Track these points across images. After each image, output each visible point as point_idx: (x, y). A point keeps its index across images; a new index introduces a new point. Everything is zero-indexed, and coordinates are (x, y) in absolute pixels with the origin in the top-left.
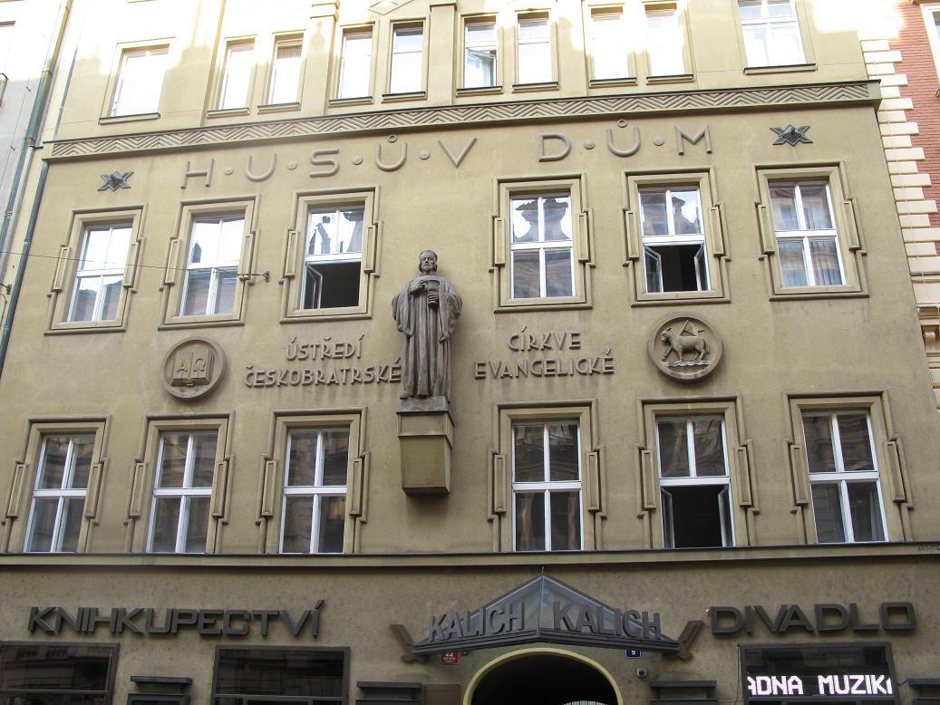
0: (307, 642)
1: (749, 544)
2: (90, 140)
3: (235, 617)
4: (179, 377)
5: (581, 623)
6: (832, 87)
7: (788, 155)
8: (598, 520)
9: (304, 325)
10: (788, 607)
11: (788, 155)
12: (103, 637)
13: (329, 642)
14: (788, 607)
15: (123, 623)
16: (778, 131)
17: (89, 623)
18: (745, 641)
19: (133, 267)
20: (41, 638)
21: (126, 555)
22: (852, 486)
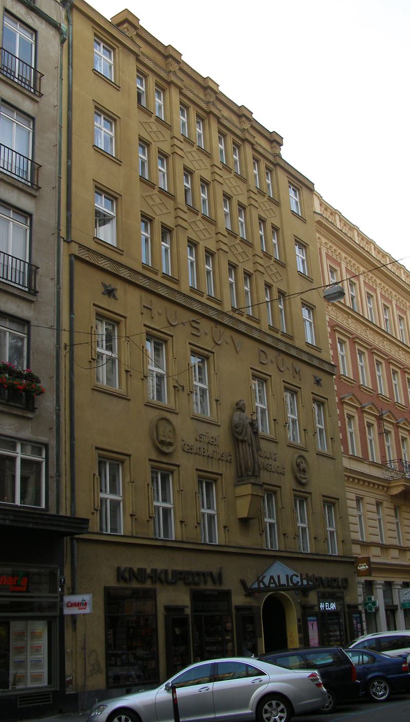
0: (218, 587)
1: (182, 539)
2: (130, 269)
3: (198, 574)
4: (163, 439)
5: (270, 583)
6: (126, 269)
7: (105, 302)
8: (183, 526)
9: (102, 394)
10: (330, 578)
11: (105, 302)
12: (148, 585)
13: (225, 587)
14: (330, 578)
15: (157, 577)
16: (105, 286)
17: (141, 575)
18: (193, 587)
19: (93, 341)
20: (123, 585)
21: (203, 544)
22: (111, 501)
